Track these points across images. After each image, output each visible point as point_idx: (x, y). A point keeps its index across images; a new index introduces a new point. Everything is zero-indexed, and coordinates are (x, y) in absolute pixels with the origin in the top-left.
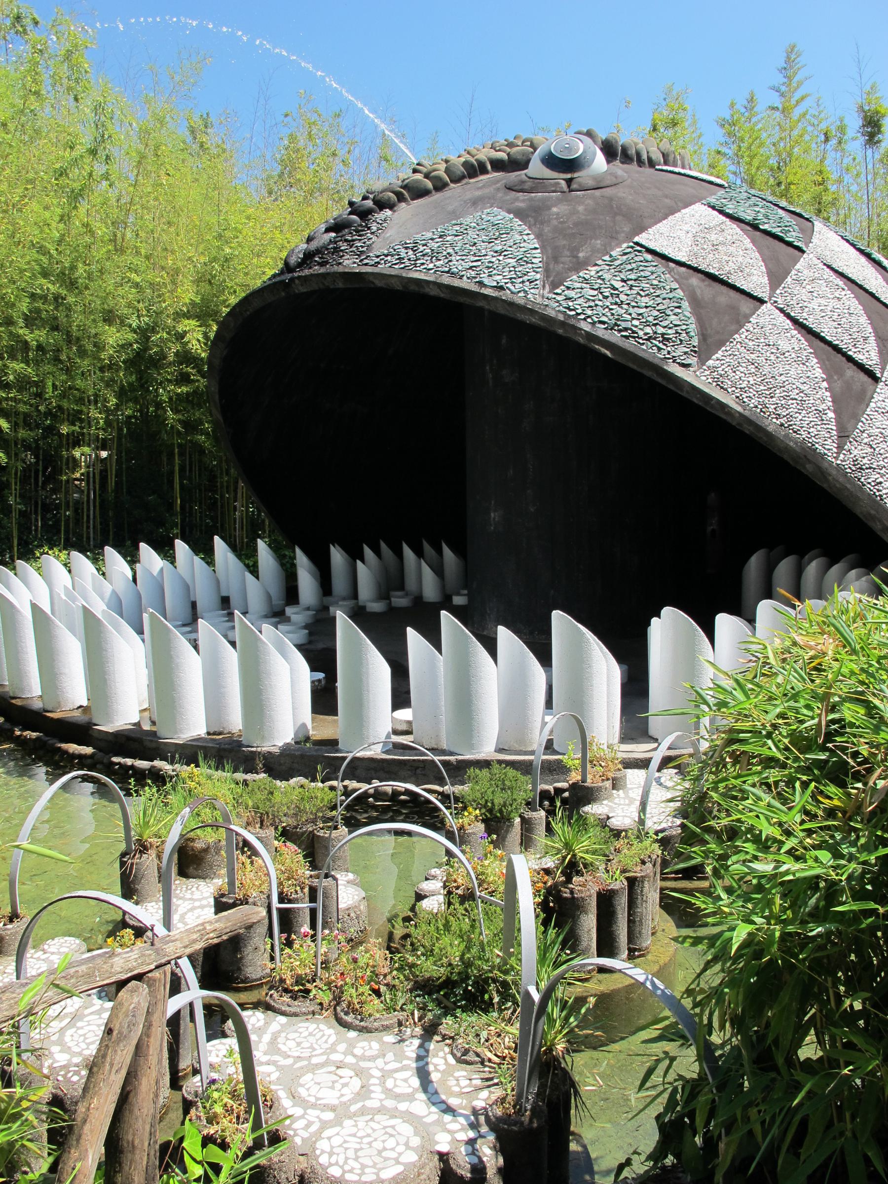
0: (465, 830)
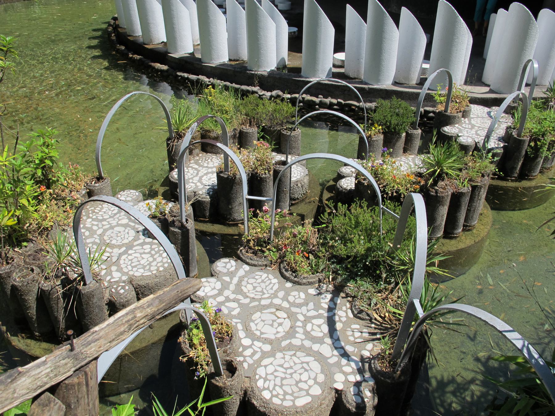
0: (371, 138)
